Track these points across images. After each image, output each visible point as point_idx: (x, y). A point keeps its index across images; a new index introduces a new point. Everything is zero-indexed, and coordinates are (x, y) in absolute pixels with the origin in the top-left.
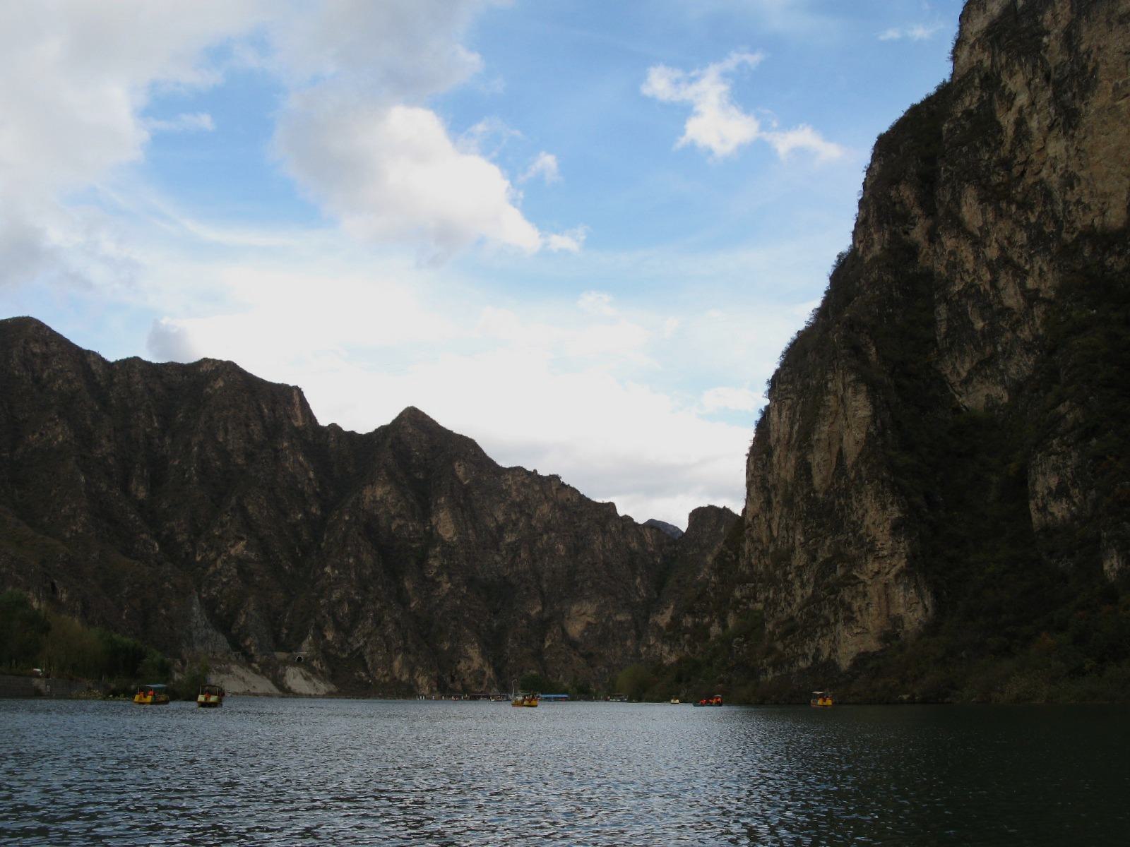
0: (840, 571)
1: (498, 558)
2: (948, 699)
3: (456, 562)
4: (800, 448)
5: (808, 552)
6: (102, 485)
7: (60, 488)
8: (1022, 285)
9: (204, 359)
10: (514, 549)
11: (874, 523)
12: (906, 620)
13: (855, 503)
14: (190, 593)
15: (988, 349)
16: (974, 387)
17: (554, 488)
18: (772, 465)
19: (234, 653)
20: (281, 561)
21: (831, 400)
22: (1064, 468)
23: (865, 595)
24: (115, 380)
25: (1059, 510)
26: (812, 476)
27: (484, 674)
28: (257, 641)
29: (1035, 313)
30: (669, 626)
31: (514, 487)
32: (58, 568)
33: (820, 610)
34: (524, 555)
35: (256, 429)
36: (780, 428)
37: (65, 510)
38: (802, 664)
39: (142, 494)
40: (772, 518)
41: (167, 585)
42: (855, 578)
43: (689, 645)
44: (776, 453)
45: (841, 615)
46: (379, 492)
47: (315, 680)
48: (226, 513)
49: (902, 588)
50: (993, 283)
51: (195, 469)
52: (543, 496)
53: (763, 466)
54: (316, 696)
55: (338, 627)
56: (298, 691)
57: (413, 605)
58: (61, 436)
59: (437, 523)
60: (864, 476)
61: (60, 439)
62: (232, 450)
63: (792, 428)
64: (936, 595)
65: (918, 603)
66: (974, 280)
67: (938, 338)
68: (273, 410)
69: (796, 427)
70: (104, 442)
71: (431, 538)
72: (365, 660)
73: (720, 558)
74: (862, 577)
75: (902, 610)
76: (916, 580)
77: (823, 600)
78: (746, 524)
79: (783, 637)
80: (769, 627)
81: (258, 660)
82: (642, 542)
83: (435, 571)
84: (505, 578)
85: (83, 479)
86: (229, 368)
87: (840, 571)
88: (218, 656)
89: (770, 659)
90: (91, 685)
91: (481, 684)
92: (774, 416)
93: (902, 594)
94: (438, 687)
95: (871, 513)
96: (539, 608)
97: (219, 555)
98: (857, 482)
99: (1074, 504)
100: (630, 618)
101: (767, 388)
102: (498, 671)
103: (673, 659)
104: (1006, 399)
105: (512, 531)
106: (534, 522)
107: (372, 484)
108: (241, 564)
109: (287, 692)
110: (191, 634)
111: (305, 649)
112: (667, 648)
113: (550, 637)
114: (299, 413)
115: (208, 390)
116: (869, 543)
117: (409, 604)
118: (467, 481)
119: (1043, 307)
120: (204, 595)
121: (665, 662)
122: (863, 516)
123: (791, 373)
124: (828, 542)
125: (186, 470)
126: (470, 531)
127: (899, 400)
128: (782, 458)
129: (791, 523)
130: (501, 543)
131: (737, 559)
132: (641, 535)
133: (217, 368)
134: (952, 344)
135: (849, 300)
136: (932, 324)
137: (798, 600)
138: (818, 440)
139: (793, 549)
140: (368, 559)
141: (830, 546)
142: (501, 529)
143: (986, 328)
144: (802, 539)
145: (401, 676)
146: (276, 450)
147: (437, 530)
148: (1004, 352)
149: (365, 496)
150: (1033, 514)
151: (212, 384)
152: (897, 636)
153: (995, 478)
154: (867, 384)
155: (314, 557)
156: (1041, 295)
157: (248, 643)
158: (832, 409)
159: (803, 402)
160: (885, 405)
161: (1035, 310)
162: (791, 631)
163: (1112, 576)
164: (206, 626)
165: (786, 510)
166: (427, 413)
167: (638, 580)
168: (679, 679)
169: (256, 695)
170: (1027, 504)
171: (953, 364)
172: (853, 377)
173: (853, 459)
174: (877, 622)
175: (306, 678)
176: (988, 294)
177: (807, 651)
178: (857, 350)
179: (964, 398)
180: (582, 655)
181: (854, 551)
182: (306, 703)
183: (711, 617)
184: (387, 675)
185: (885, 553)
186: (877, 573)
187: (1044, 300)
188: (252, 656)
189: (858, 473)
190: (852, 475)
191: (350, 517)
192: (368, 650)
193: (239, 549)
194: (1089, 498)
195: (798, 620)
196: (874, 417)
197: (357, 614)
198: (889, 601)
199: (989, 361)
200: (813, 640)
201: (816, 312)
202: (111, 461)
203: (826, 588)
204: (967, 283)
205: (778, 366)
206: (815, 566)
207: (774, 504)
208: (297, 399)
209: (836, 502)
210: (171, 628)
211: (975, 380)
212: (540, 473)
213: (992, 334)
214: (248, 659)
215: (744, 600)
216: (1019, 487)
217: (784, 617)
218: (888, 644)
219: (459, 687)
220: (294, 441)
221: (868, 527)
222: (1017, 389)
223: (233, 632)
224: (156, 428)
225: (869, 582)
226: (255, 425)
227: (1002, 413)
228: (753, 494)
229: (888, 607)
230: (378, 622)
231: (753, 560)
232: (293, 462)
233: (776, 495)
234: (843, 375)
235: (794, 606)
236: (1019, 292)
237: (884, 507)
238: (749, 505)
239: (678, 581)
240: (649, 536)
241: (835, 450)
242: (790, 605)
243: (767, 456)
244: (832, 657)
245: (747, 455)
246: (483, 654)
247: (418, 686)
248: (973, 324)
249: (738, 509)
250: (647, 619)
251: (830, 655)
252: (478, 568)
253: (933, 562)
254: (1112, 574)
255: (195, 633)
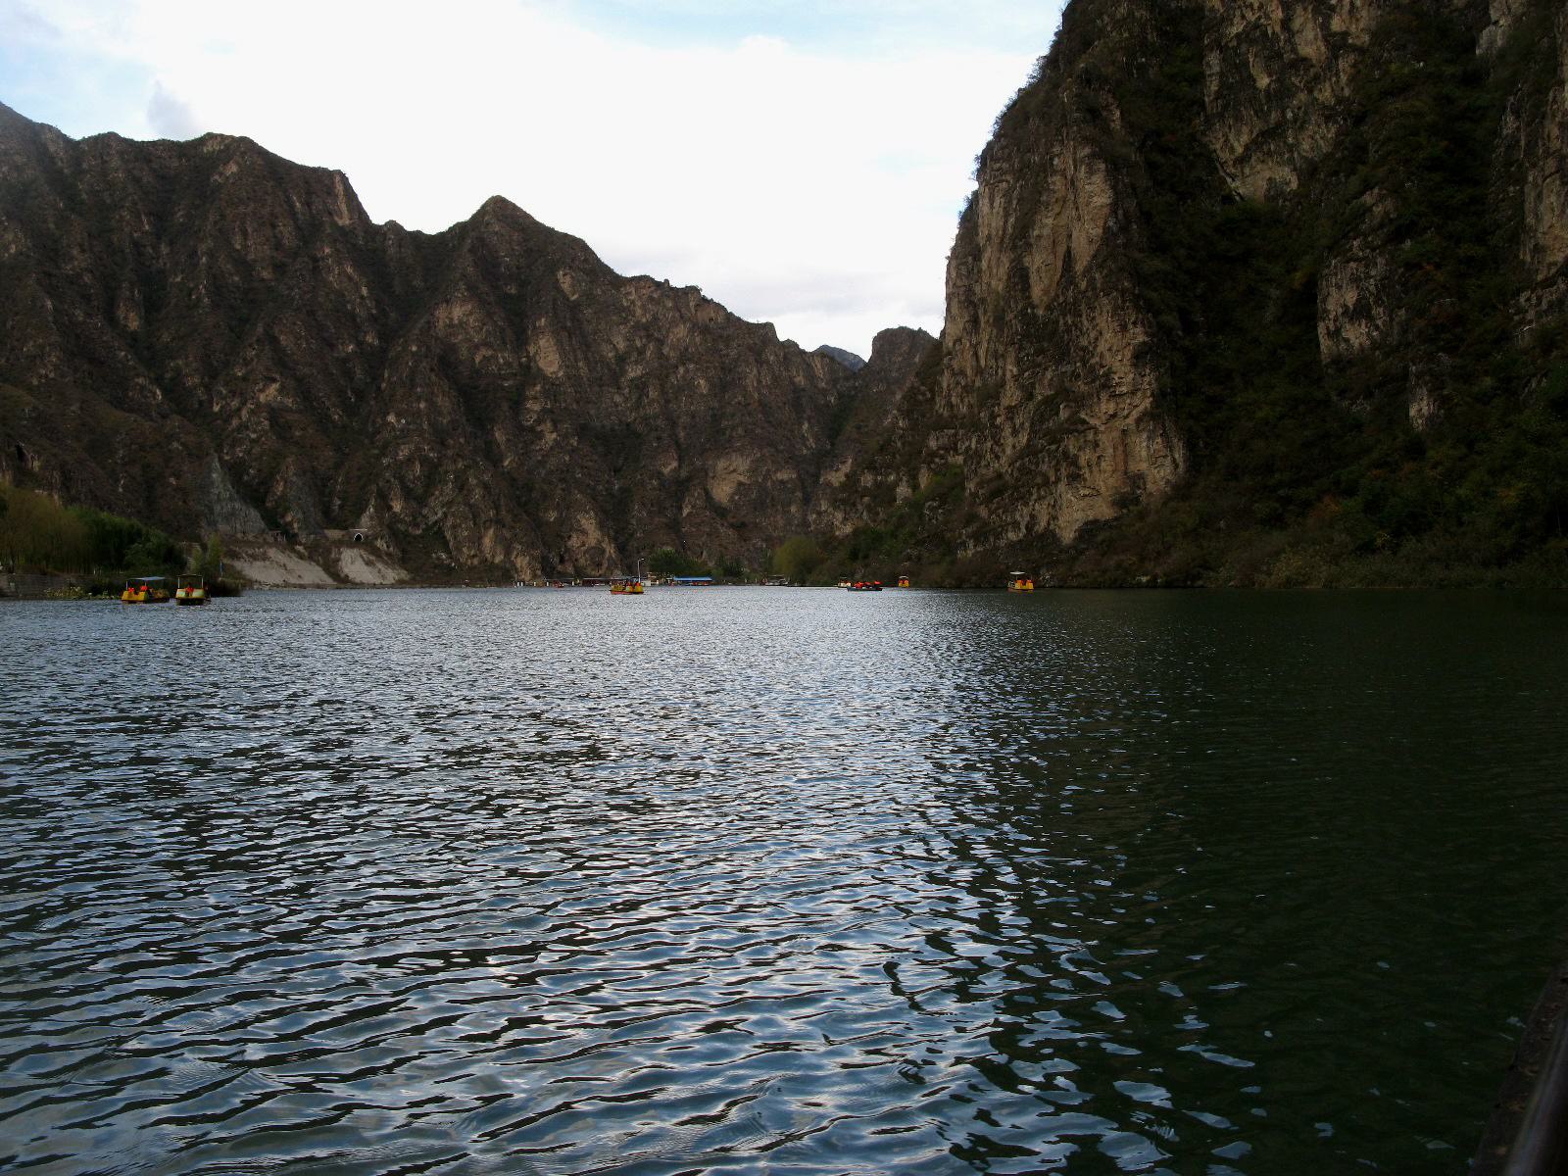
0: (1064, 414)
1: (618, 399)
2: (1200, 583)
3: (563, 405)
4: (1014, 247)
5: (1022, 387)
6: (77, 312)
7: (18, 317)
8: (1325, 26)
9: (208, 134)
10: (640, 386)
11: (1110, 350)
12: (1149, 479)
13: (1085, 322)
14: (207, 454)
15: (1274, 116)
16: (1252, 168)
17: (692, 304)
18: (980, 271)
19: (270, 533)
20: (328, 409)
21: (1057, 183)
22: (1366, 278)
23: (1096, 445)
24: (85, 166)
25: (1357, 335)
26: (1029, 286)
27: (603, 551)
28: (300, 516)
29: (1340, 67)
30: (844, 487)
31: (639, 303)
32: (25, 426)
33: (1037, 464)
34: (653, 394)
35: (286, 231)
36: (992, 221)
37: (29, 347)
38: (1012, 536)
39: (134, 323)
40: (978, 343)
41: (175, 445)
42: (1084, 422)
43: (869, 512)
44: (986, 255)
45: (1064, 472)
46: (457, 312)
47: (380, 566)
48: (250, 345)
49: (1145, 436)
50: (1286, 23)
51: (205, 287)
52: (677, 315)
53: (969, 272)
54: (382, 586)
55: (408, 494)
56: (358, 580)
57: (506, 463)
58: (14, 246)
59: (536, 353)
60: (1099, 285)
61: (13, 250)
62: (255, 261)
63: (1006, 222)
64: (1191, 446)
65: (1165, 457)
66: (1259, 18)
67: (1206, 99)
68: (308, 204)
69: (1012, 220)
70: (75, 252)
71: (528, 373)
72: (444, 537)
73: (911, 395)
74: (1092, 422)
75: (1144, 466)
76: (1164, 426)
77: (1041, 452)
78: (945, 350)
79: (988, 500)
80: (971, 486)
81: (304, 541)
82: (811, 377)
83: (535, 417)
84: (628, 425)
85: (49, 304)
86: (244, 147)
87: (1064, 414)
88: (250, 537)
89: (970, 530)
90: (73, 581)
91: (599, 565)
92: (984, 206)
93: (1144, 444)
94: (543, 570)
95: (1108, 335)
96: (675, 464)
97: (244, 403)
98: (1090, 294)
99: (1377, 328)
100: (794, 476)
101: (975, 166)
102: (621, 549)
103: (848, 529)
104: (1294, 185)
105: (636, 362)
106: (666, 350)
107: (447, 302)
108: (274, 414)
109: (343, 582)
110: (211, 511)
111: (365, 526)
112: (839, 516)
113: (690, 503)
114: (344, 207)
115: (217, 177)
116: (1102, 376)
117: (502, 462)
118: (576, 297)
119: (1352, 58)
120: (227, 458)
121: (837, 533)
122: (1097, 339)
123: (1006, 147)
124: (1049, 375)
125: (193, 289)
126: (581, 364)
127: (1150, 184)
128: (993, 263)
129: (1001, 349)
130: (623, 380)
131: (933, 398)
132: (809, 365)
133: (227, 147)
134: (1225, 107)
135: (1087, 44)
136: (1198, 79)
137: (1009, 451)
138: (1038, 236)
139: (1002, 384)
140: (444, 402)
141: (1052, 379)
142: (622, 359)
143: (1273, 86)
144: (1015, 370)
145: (493, 556)
146: (315, 260)
147: (535, 362)
148: (1295, 121)
149: (438, 318)
150: (1322, 340)
151: (221, 169)
152: (1136, 501)
153: (1274, 293)
154: (1105, 161)
155: (372, 403)
156: (1350, 41)
157: (289, 519)
158: (1059, 195)
159: (1021, 186)
160: (1130, 190)
161: (1340, 61)
162: (997, 493)
163: (1419, 424)
164: (231, 499)
165: (995, 331)
166: (519, 204)
167: (806, 426)
168: (854, 556)
169: (302, 587)
170: (1315, 328)
171: (1225, 135)
172: (1087, 151)
173: (1085, 263)
174: (1111, 481)
175: (368, 563)
176: (1278, 37)
177: (1018, 517)
178: (1094, 114)
179: (1238, 183)
180: (732, 526)
181: (1082, 386)
182: (373, 595)
183: (898, 474)
184: (474, 556)
185: (1124, 389)
186: (1114, 416)
187: (1355, 49)
188: (295, 535)
189: (1092, 282)
190: (1083, 285)
191: (419, 347)
192: (449, 524)
193: (270, 394)
194: (1397, 319)
195: (1007, 477)
196: (1114, 207)
197: (432, 478)
198: (1127, 455)
199: (1274, 133)
200: (1026, 504)
201: (1041, 61)
202: (87, 278)
203: (1045, 436)
204: (1249, 23)
205: (990, 137)
206: (1031, 406)
207: (983, 325)
208: (340, 188)
209: (1062, 322)
210: (184, 502)
211: (1254, 158)
212: (674, 283)
213: (1280, 94)
214: (290, 540)
215: (942, 452)
216: (1305, 305)
217: (990, 473)
218: (1125, 511)
219: (570, 570)
220: (339, 246)
221: (1102, 356)
222: (1309, 172)
223: (269, 505)
224: (147, 232)
225: (1102, 428)
226: (284, 225)
227: (1287, 203)
228: (955, 311)
229: (1126, 463)
230: (461, 486)
231: (953, 399)
232: (339, 274)
233: (985, 312)
234: (1075, 148)
235: (1003, 460)
236: (1320, 36)
237: (1124, 328)
238: (948, 326)
239: (859, 428)
240: (819, 366)
241: (1061, 250)
242: (997, 457)
243: (974, 259)
244: (1052, 527)
245: (948, 258)
246: (601, 526)
247: (516, 569)
248: (1254, 81)
249: (935, 327)
250: (817, 476)
251: (1049, 524)
252: (592, 412)
253: (1188, 400)
254: (1420, 421)
255: (217, 508)
